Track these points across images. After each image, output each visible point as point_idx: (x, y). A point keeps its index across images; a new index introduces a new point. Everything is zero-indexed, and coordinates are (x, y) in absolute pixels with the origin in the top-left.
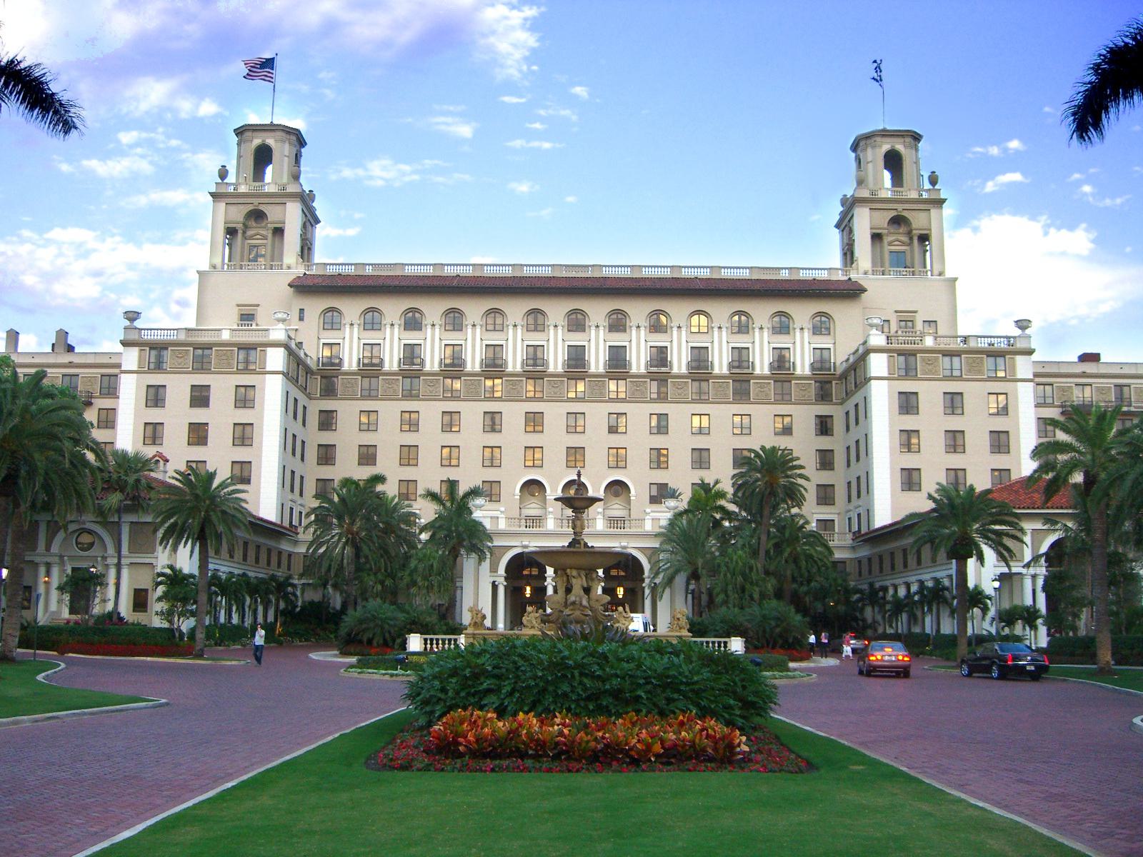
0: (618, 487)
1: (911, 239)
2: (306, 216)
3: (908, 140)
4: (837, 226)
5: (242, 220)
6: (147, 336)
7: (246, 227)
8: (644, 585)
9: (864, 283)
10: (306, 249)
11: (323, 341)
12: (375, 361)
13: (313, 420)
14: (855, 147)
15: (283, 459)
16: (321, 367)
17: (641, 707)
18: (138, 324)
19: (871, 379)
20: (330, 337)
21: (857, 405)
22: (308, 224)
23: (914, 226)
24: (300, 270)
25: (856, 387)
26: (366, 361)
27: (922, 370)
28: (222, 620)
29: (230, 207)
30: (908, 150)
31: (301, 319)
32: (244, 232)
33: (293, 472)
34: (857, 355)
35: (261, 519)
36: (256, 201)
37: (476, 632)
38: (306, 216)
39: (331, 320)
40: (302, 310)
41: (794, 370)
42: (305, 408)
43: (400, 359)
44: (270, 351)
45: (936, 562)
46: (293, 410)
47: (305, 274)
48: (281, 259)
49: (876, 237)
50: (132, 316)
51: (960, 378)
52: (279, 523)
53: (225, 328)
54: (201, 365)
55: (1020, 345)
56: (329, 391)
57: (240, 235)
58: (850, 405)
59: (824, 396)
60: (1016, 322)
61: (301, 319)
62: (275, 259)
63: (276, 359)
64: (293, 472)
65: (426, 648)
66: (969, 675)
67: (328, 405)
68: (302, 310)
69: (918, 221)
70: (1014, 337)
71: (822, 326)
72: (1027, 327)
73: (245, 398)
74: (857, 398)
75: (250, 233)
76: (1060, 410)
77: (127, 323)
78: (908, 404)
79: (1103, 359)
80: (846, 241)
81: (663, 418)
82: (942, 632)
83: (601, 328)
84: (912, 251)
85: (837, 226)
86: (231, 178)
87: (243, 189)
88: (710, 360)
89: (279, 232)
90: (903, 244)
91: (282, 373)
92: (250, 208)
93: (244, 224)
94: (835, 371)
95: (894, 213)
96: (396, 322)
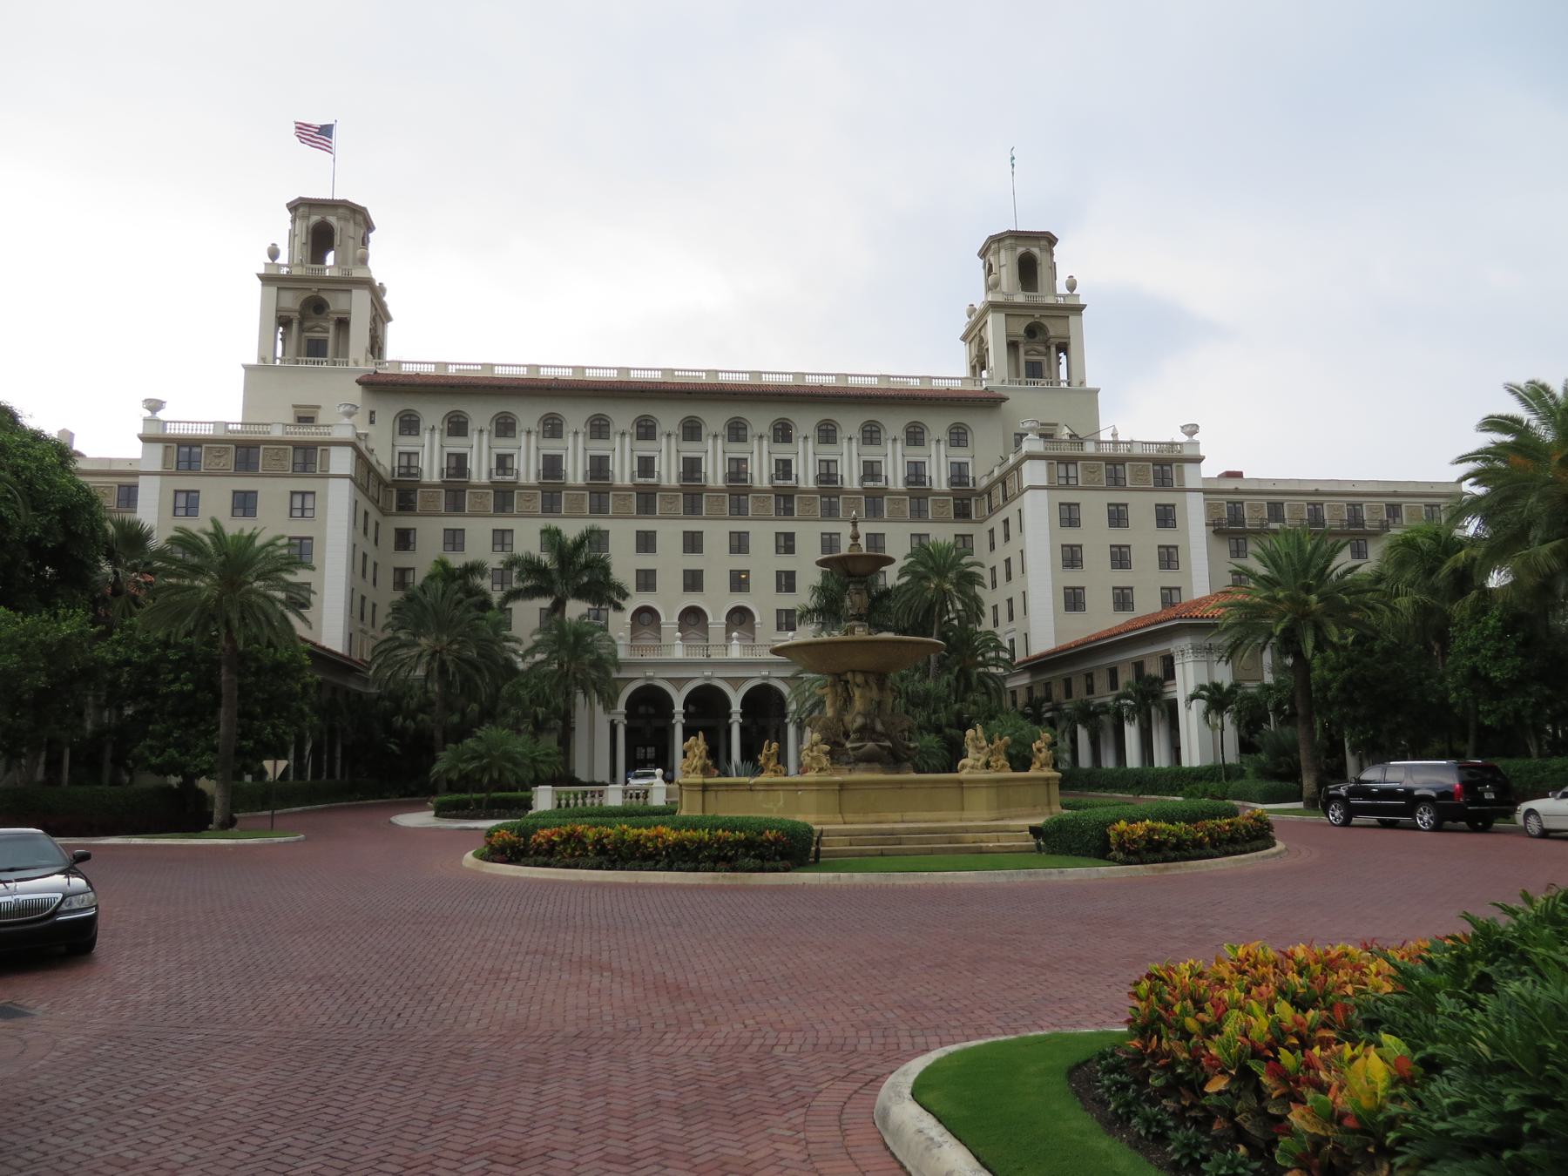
0: (693, 618)
1: (1048, 348)
2: (376, 309)
3: (1044, 243)
4: (964, 338)
5: (297, 307)
6: (172, 430)
7: (303, 318)
8: (787, 720)
9: (1005, 394)
10: (376, 346)
11: (400, 449)
12: (413, 471)
13: (389, 539)
14: (983, 254)
15: (352, 582)
16: (396, 477)
17: (1527, 978)
18: (161, 415)
19: (1022, 492)
20: (407, 443)
21: (1006, 522)
22: (378, 319)
23: (1052, 333)
24: (371, 367)
25: (1005, 498)
26: (402, 471)
27: (263, 466)
28: (1133, 760)
29: (1009, 319)
30: (1044, 254)
31: (372, 422)
32: (301, 324)
33: (363, 598)
34: (1006, 467)
35: (323, 648)
36: (315, 287)
37: (709, 781)
38: (376, 309)
39: (409, 424)
40: (372, 413)
41: (842, 483)
42: (377, 524)
43: (443, 470)
44: (334, 450)
45: (1092, 693)
46: (362, 524)
47: (376, 372)
48: (346, 355)
49: (1013, 346)
50: (154, 405)
51: (1076, 488)
52: (346, 654)
53: (279, 428)
54: (1116, 482)
55: (1187, 452)
56: (406, 504)
57: (295, 326)
58: (996, 522)
59: (962, 513)
60: (1182, 427)
61: (372, 422)
62: (342, 351)
63: (341, 461)
64: (363, 598)
65: (559, 806)
66: (1346, 823)
67: (405, 522)
68: (372, 413)
69: (1054, 329)
70: (1181, 444)
71: (958, 437)
72: (1195, 432)
73: (302, 504)
74: (1009, 512)
75: (307, 324)
76: (1212, 528)
77: (148, 414)
78: (1069, 516)
79: (1245, 476)
80: (974, 352)
81: (790, 537)
82: (1185, 763)
83: (854, 441)
84: (1049, 360)
85: (964, 338)
86: (283, 258)
87: (297, 272)
88: (839, 473)
89: (343, 324)
90: (1039, 353)
91: (349, 477)
92: (308, 294)
93: (300, 313)
94: (974, 485)
95: (1030, 321)
96: (439, 425)
